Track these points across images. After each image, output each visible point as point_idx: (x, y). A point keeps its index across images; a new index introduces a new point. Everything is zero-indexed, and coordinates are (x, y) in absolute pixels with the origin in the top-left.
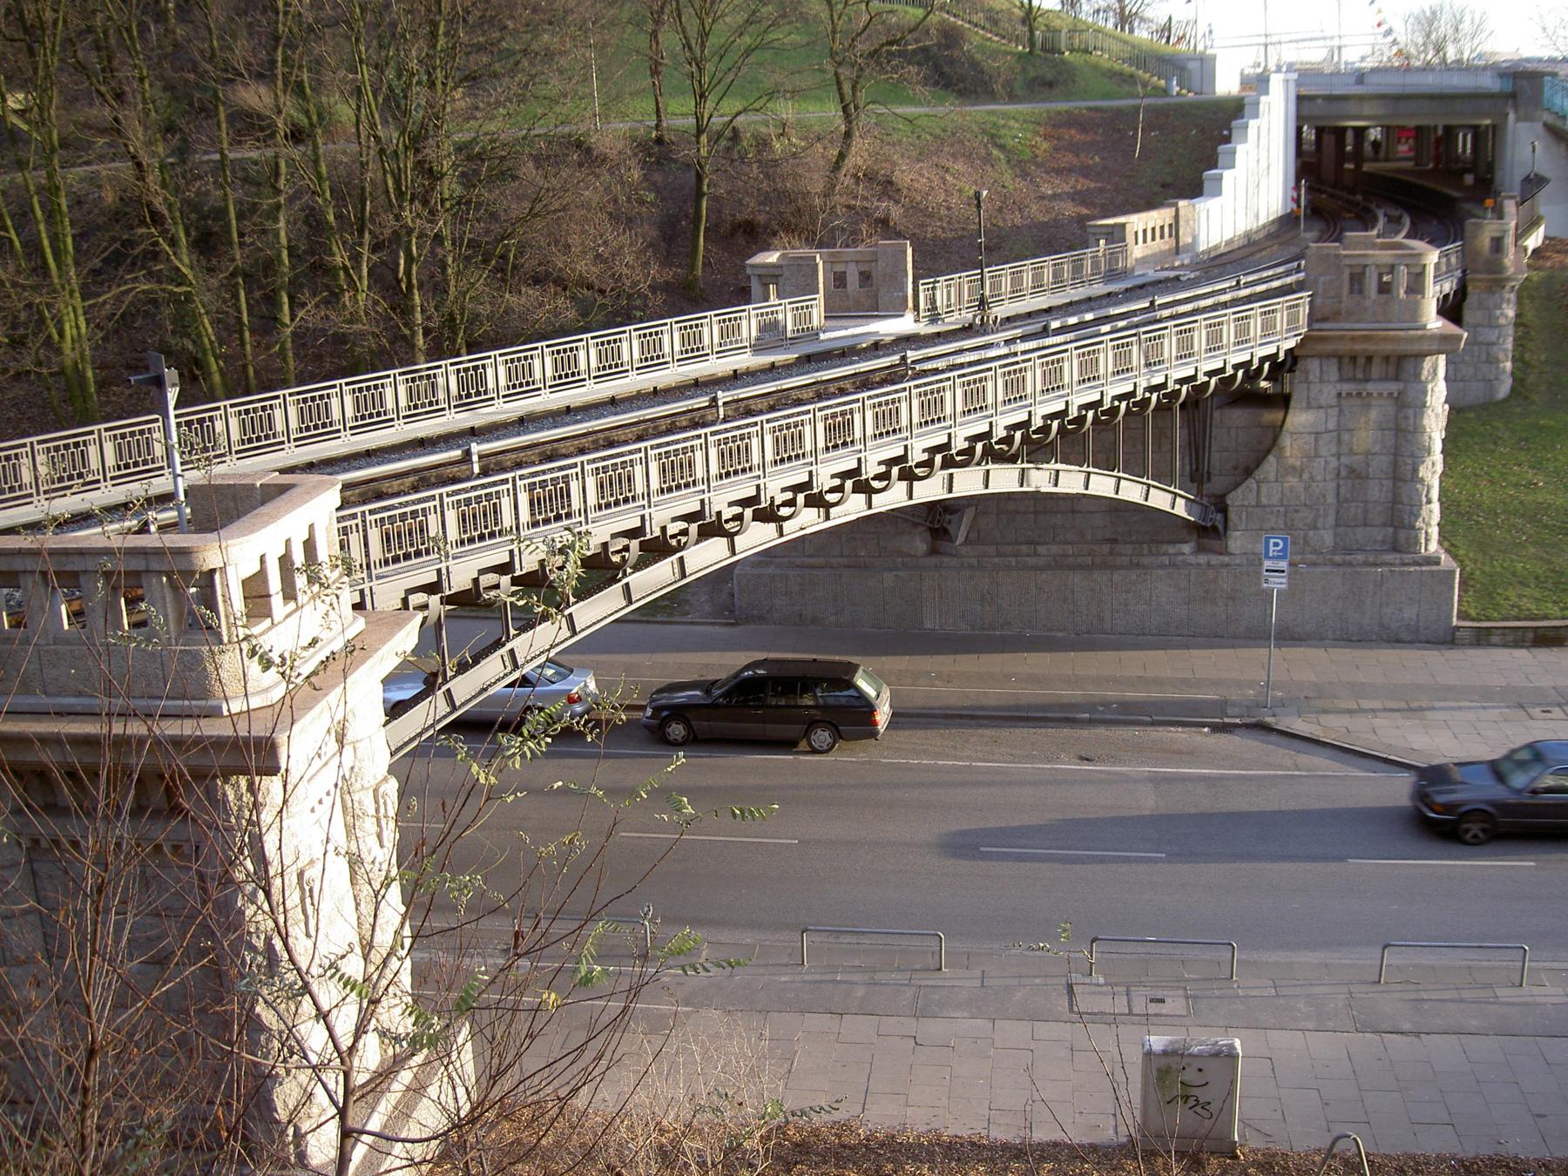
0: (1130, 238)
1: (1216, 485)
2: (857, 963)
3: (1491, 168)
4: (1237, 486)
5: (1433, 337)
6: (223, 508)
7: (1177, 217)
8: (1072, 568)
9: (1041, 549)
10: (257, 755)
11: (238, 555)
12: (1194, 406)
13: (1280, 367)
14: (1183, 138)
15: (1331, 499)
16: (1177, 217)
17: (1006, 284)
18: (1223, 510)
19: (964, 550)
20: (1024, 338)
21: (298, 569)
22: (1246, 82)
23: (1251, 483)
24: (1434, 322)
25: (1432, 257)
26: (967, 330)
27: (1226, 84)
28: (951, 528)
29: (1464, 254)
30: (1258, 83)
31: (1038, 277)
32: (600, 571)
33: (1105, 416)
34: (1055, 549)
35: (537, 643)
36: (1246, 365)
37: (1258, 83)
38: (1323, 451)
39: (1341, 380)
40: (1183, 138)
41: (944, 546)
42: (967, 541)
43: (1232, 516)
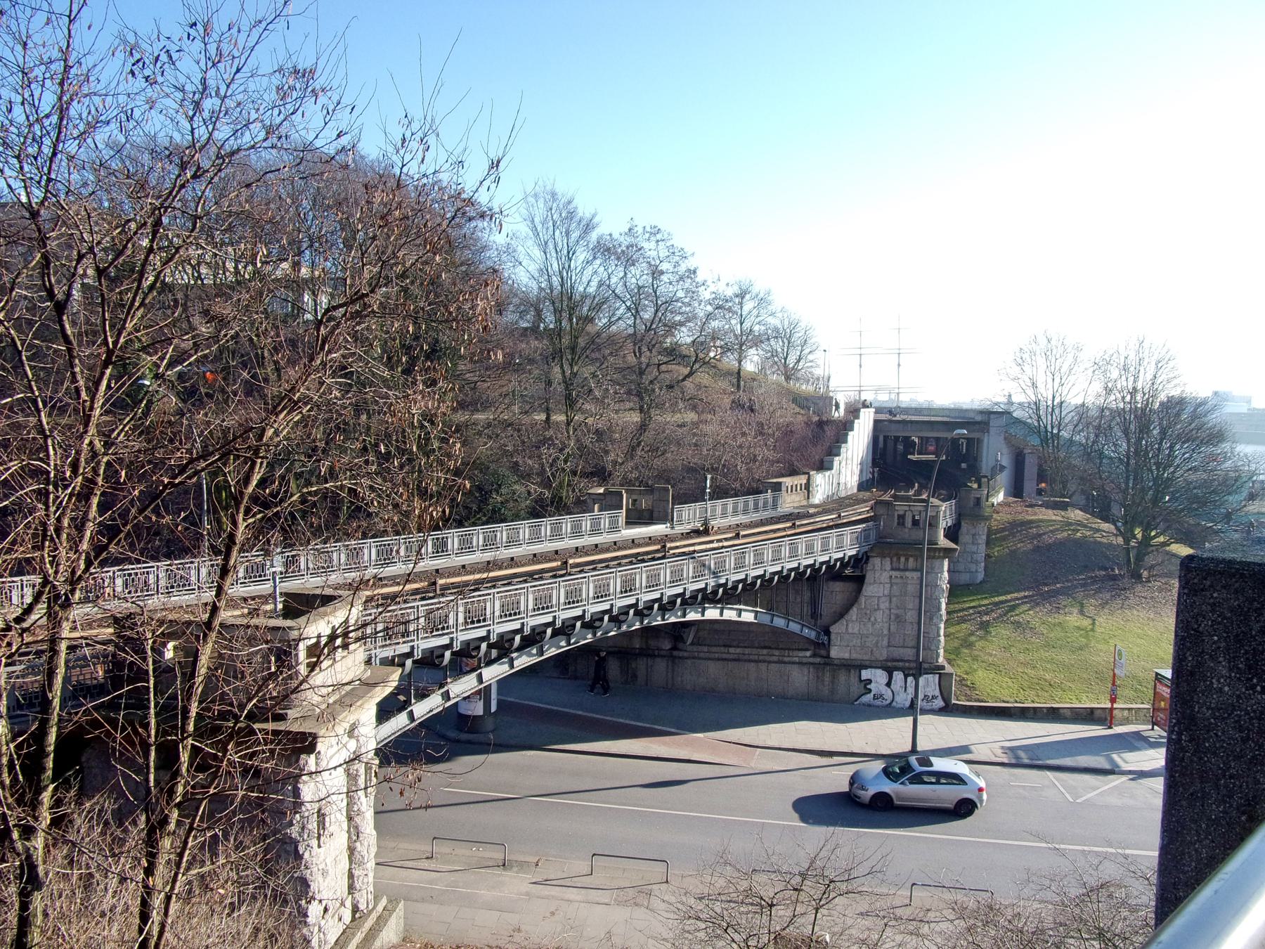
0: (784, 489)
1: (825, 620)
2: (592, 284)
3: (976, 459)
4: (835, 622)
5: (940, 549)
6: (300, 605)
7: (809, 480)
8: (750, 661)
9: (732, 650)
10: (305, 743)
11: (318, 627)
12: (812, 580)
13: (859, 562)
14: (819, 436)
15: (886, 632)
16: (809, 480)
17: (719, 510)
18: (827, 632)
19: (689, 648)
20: (726, 539)
21: (338, 640)
22: (848, 411)
23: (843, 621)
24: (943, 542)
25: (944, 507)
26: (697, 533)
27: (839, 414)
28: (685, 636)
29: (958, 506)
30: (853, 411)
31: (756, 505)
32: (503, 647)
33: (766, 581)
34: (738, 650)
35: (462, 687)
36: (842, 559)
37: (853, 411)
38: (882, 606)
39: (892, 569)
40: (819, 436)
41: (680, 645)
42: (692, 644)
43: (833, 637)
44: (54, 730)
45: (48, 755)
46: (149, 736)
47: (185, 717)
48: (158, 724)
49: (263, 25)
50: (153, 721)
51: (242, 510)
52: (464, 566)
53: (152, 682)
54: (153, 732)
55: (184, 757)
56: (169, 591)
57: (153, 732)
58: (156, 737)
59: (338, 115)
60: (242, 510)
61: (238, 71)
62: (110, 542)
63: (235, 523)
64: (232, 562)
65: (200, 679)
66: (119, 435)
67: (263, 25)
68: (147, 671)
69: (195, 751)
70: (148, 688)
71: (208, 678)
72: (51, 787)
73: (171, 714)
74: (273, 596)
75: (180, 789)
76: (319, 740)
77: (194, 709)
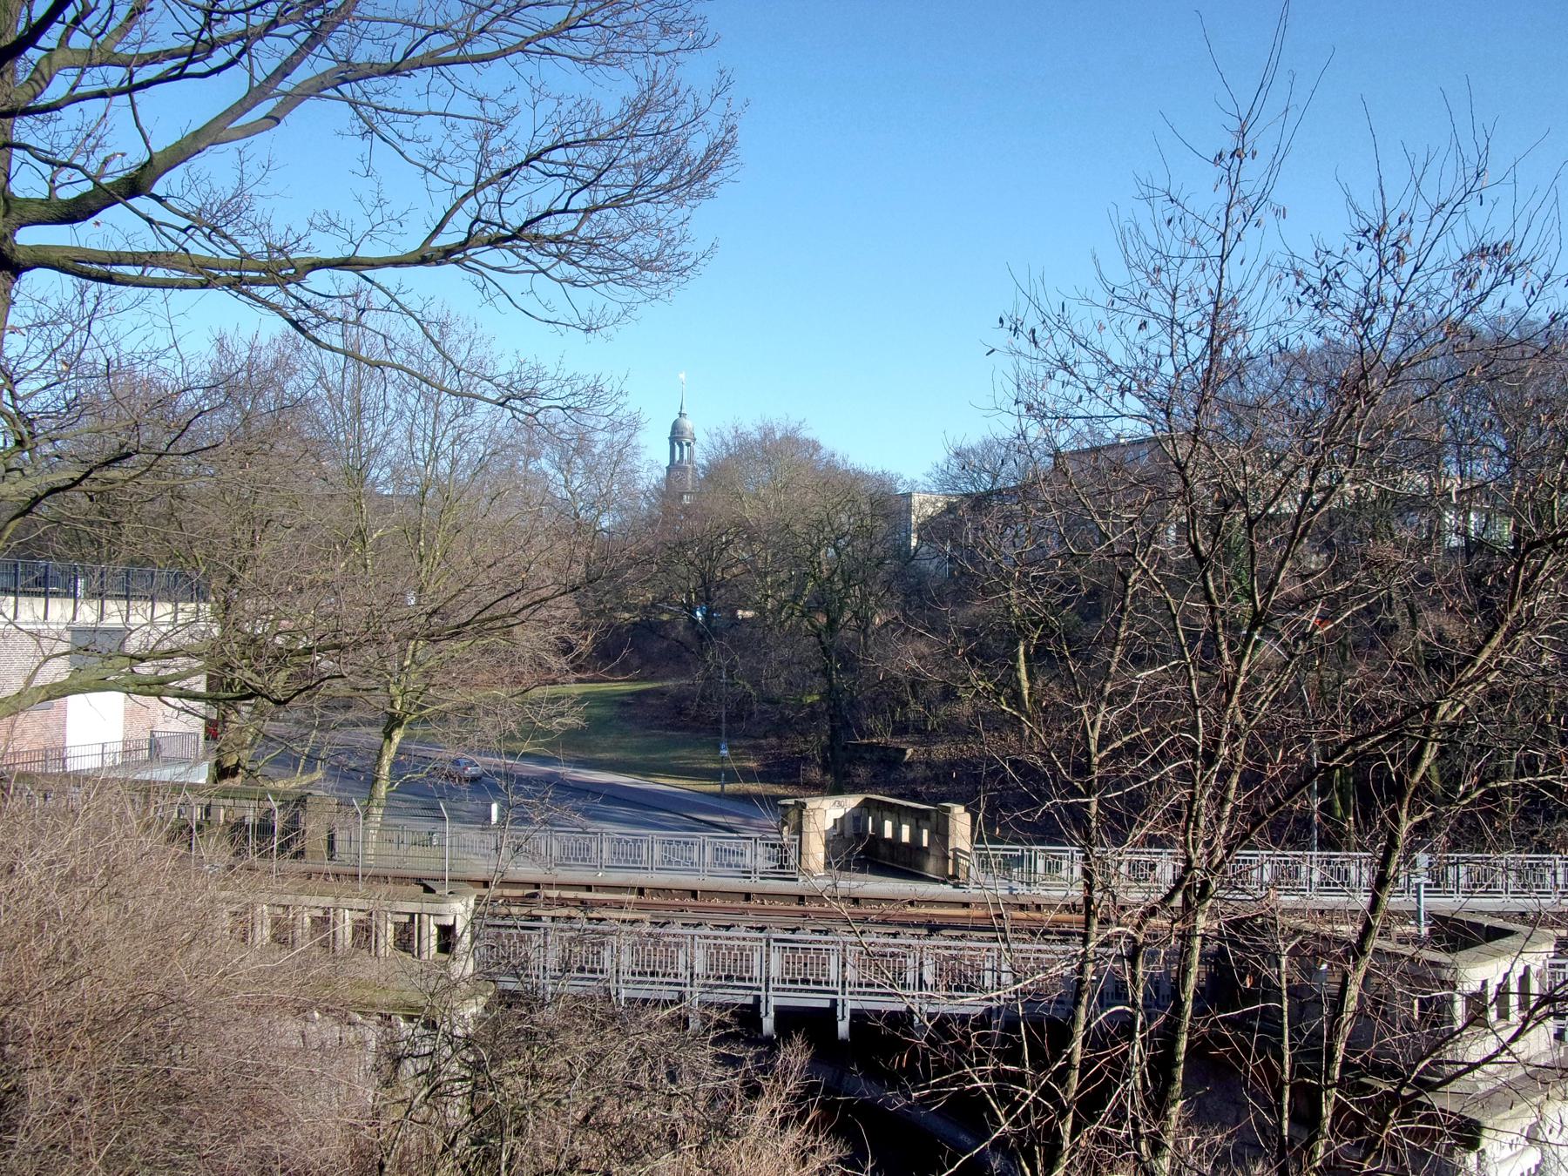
6: (1460, 935)
11: (1482, 972)
44: (1185, 1037)
45: (1178, 1065)
46: (1283, 1071)
47: (1331, 1058)
48: (1294, 1058)
49: (1449, 208)
50: (1287, 1054)
51: (1406, 805)
52: (1523, 914)
53: (1286, 1004)
54: (1287, 1067)
55: (1327, 1111)
56: (1306, 892)
57: (1287, 1067)
58: (1291, 1075)
59: (1548, 291)
60: (1406, 805)
61: (1416, 269)
62: (1252, 829)
63: (1397, 821)
64: (1392, 871)
65: (1350, 1015)
66: (1262, 704)
67: (1449, 208)
68: (1280, 989)
69: (1340, 1108)
70: (1281, 1011)
71: (1359, 1013)
72: (1180, 1103)
73: (1313, 1054)
74: (1415, 915)
75: (1321, 1150)
76: (1486, 1133)
77: (1340, 1048)
